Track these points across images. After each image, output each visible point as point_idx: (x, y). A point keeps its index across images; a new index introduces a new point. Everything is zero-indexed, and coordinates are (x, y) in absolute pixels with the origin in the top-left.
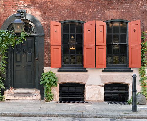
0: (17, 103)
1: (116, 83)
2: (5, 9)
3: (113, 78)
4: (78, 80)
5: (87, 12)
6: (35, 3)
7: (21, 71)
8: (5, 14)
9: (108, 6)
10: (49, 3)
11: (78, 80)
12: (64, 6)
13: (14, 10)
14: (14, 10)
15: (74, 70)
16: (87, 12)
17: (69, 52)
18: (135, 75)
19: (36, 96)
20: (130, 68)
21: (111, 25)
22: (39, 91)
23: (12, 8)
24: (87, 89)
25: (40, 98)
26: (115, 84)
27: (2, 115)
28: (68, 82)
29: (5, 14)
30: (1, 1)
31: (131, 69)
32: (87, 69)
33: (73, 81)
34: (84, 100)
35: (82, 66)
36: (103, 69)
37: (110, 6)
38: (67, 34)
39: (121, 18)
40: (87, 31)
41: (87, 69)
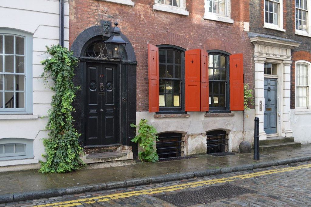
2: (79, 16)
4: (179, 128)
7: (292, 106)
8: (78, 24)
11: (179, 128)
13: (91, 19)
14: (91, 19)
18: (258, 119)
19: (128, 155)
22: (131, 147)
23: (89, 16)
25: (132, 158)
26: (209, 132)
27: (6, 202)
28: (166, 132)
29: (78, 24)
30: (72, 1)
33: (173, 130)
38: (174, 66)
39: (120, 57)
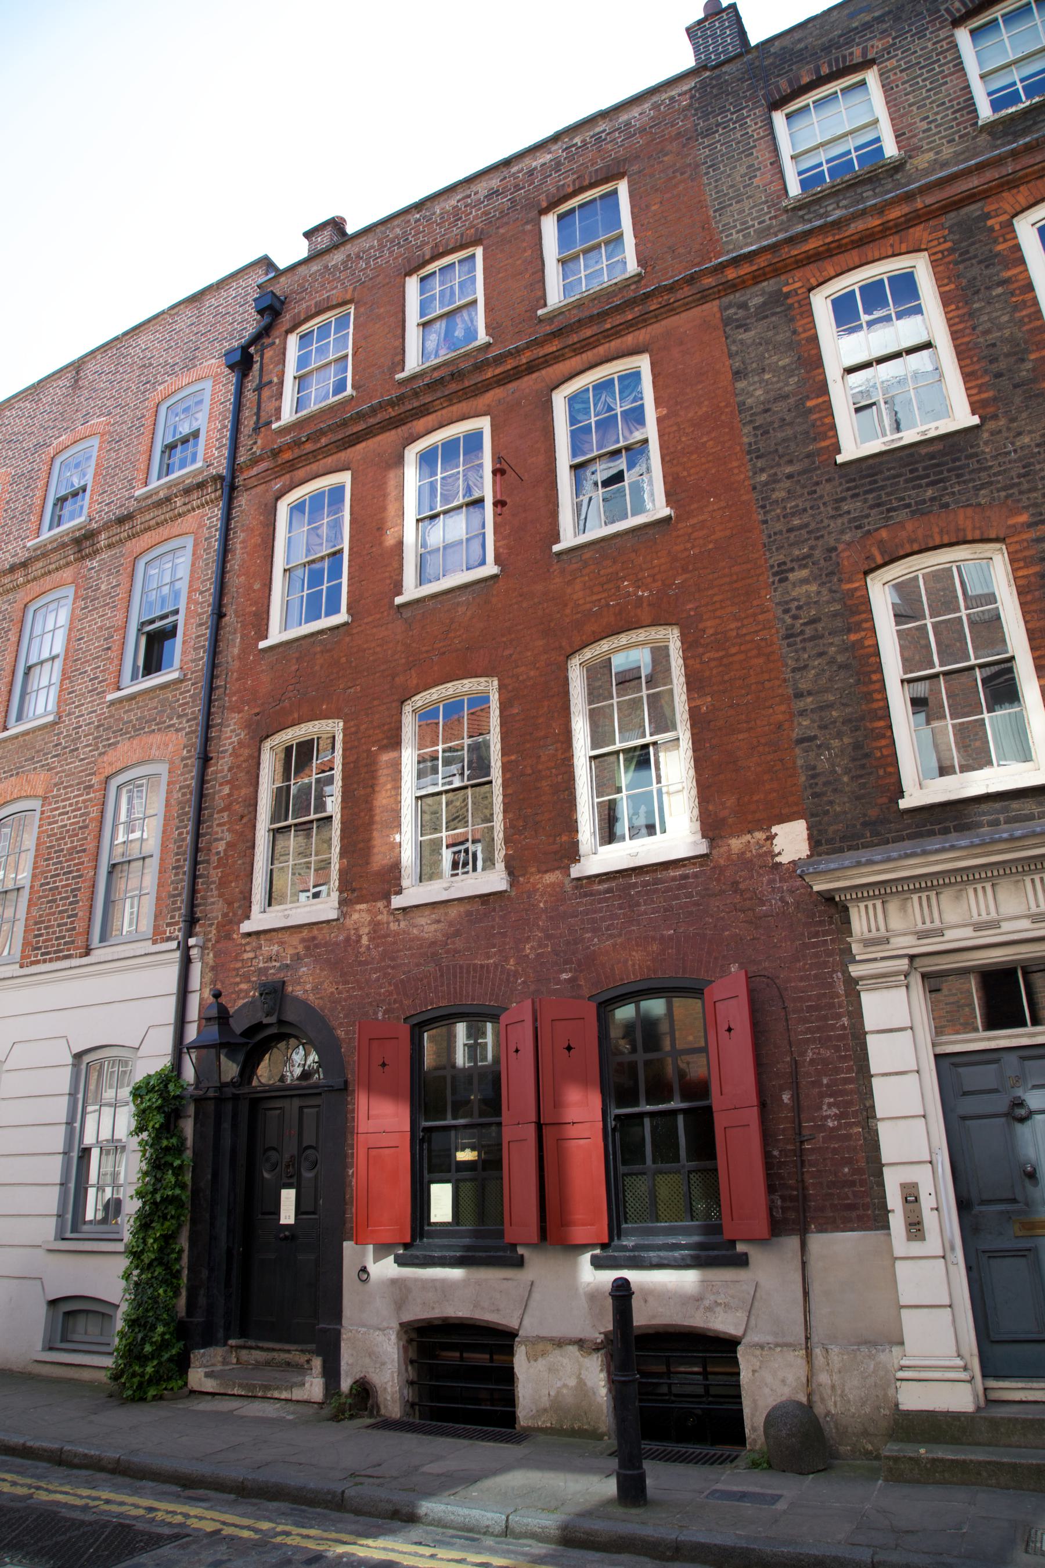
0: (218, 1413)
1: (500, 1328)
3: (646, 1301)
4: (483, 1308)
5: (512, 962)
6: (316, 946)
9: (603, 920)
10: (365, 941)
12: (421, 947)
15: (444, 1258)
16: (512, 962)
17: (453, 1168)
20: (733, 1243)
21: (625, 1013)
24: (746, 1361)
31: (740, 1248)
32: (740, 1248)
34: (509, 1419)
35: (501, 1234)
36: (598, 1251)
37: (613, 917)
40: (512, 1054)
41: (521, 1250)
